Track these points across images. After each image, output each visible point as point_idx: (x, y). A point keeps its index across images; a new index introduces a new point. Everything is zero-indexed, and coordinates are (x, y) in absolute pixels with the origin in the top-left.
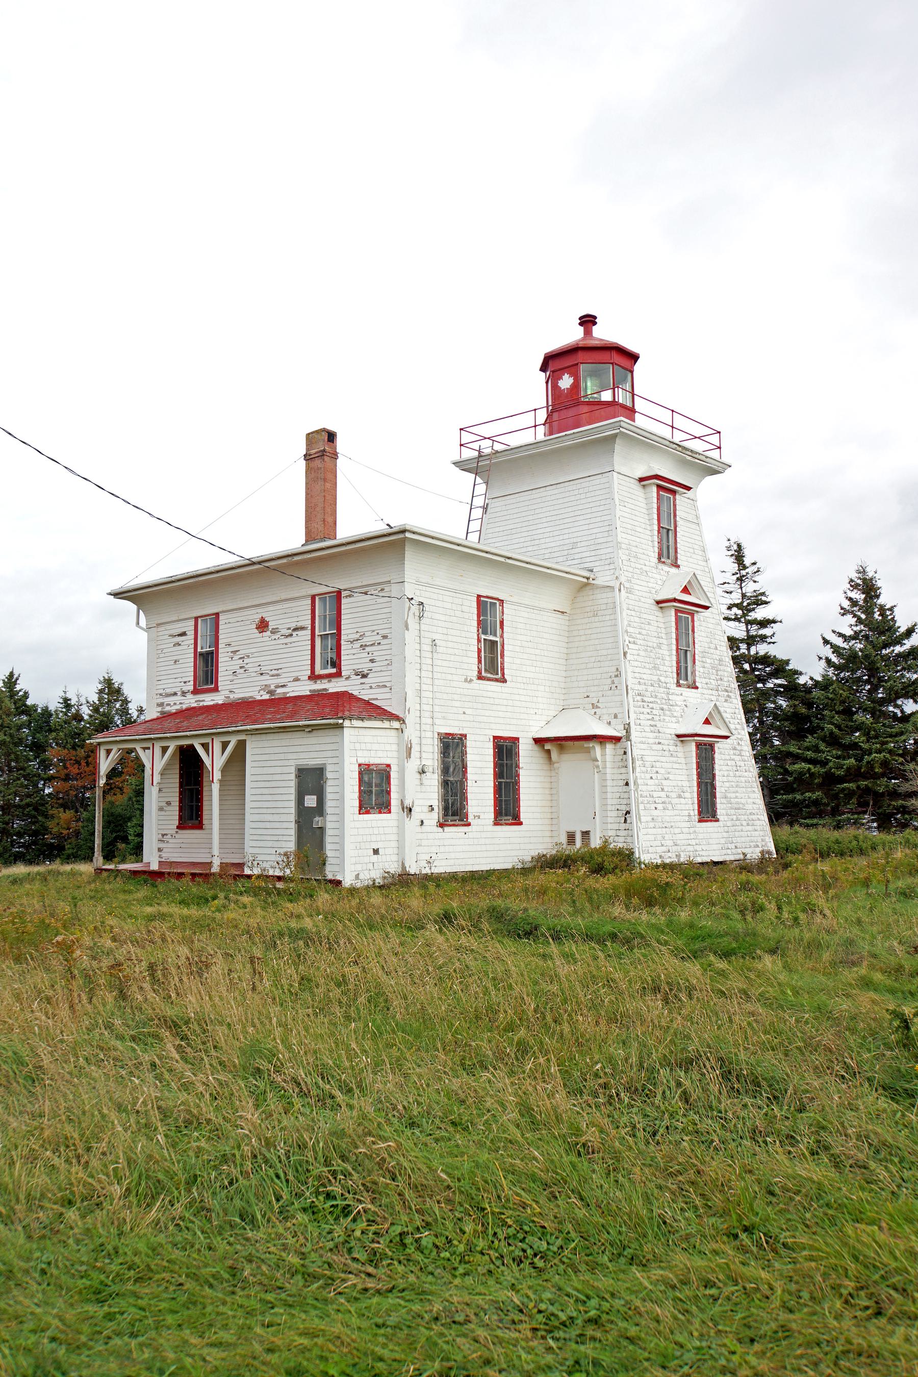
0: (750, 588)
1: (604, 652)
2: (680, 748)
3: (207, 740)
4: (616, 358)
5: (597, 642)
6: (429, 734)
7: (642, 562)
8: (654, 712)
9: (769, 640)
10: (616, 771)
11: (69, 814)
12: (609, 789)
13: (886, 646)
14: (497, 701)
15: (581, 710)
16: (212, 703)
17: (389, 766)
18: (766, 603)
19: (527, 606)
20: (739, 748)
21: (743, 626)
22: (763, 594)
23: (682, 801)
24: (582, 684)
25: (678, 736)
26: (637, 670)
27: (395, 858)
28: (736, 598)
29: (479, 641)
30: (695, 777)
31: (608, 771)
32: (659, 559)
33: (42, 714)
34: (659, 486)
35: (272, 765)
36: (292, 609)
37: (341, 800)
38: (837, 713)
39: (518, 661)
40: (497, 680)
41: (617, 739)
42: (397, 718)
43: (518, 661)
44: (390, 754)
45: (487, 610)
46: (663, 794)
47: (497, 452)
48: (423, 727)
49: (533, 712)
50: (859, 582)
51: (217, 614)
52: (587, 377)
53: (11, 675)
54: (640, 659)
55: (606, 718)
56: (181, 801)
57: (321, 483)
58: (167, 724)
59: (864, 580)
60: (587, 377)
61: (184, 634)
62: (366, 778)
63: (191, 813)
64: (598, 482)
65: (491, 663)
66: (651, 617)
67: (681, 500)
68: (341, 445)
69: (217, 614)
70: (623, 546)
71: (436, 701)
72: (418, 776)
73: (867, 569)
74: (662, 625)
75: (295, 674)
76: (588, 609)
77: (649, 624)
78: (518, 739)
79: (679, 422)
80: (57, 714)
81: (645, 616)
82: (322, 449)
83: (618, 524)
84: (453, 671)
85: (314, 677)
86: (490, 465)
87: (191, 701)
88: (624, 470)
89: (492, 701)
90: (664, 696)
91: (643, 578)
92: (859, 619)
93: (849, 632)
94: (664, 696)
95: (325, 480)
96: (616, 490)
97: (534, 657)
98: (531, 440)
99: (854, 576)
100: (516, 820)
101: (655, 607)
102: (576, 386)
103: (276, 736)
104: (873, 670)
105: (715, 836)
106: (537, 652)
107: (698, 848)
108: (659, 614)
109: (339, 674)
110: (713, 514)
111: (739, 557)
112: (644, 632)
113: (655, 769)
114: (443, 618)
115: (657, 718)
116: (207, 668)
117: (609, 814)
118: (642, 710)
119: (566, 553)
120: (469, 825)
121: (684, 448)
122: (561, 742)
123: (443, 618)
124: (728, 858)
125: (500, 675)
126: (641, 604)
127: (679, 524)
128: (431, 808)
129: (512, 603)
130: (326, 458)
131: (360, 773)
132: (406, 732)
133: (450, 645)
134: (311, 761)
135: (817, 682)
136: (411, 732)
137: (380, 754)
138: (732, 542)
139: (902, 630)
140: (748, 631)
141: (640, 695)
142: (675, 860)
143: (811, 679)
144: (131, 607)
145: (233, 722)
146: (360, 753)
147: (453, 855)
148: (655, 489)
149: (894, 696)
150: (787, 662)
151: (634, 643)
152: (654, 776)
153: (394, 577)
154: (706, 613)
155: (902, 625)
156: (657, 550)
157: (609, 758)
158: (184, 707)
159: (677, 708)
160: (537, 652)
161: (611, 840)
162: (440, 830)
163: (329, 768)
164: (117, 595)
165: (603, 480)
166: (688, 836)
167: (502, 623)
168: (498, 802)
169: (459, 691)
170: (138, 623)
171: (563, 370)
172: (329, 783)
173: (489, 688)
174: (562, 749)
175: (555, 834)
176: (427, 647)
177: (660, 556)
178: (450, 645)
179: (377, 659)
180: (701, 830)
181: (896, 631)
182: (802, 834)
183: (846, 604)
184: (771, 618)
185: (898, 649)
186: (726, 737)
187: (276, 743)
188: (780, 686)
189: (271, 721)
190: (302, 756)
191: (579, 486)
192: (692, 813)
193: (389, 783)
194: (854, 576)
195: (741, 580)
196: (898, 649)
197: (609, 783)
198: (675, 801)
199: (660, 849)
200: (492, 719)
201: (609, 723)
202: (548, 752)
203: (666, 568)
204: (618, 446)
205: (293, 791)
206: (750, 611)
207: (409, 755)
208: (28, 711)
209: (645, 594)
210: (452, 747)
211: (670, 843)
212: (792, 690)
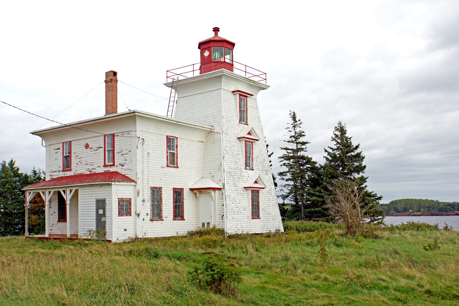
0: (298, 130)
1: (217, 157)
2: (245, 192)
3: (44, 191)
4: (225, 44)
5: (214, 153)
6: (147, 187)
7: (232, 123)
8: (235, 179)
9: (304, 150)
10: (219, 200)
11: (36, 216)
12: (217, 207)
13: (348, 153)
14: (175, 175)
15: (208, 178)
16: (69, 175)
17: (130, 199)
18: (304, 136)
19: (187, 140)
20: (270, 192)
21: (295, 145)
22: (303, 132)
23: (245, 211)
24: (209, 168)
25: (245, 188)
26: (228, 164)
27: (133, 232)
28: (293, 134)
29: (167, 152)
30: (251, 203)
31: (216, 200)
32: (240, 122)
33: (25, 177)
34: (240, 95)
35: (87, 198)
36: (97, 141)
37: (111, 211)
38: (328, 178)
39: (183, 160)
40: (175, 167)
41: (220, 189)
42: (134, 181)
43: (183, 160)
44: (131, 195)
45: (171, 142)
46: (237, 209)
47: (179, 80)
48: (144, 185)
49: (189, 179)
50: (339, 128)
51: (71, 142)
52: (215, 51)
53: (12, 161)
54: (230, 159)
55: (216, 181)
56: (59, 212)
57: (111, 92)
58: (52, 183)
59: (341, 127)
60: (215, 51)
61: (59, 149)
62: (121, 203)
63: (62, 217)
64: (216, 93)
65: (172, 161)
66: (235, 144)
67: (250, 100)
68: (119, 77)
69: (113, 135)
70: (225, 117)
71: (150, 175)
72: (142, 202)
73: (342, 123)
74: (240, 147)
75: (99, 165)
76: (211, 141)
78: (183, 189)
79: (248, 70)
80: (31, 177)
81: (232, 143)
82: (111, 78)
83: (223, 109)
84: (157, 164)
85: (105, 166)
86: (177, 86)
87: (62, 174)
88: (226, 88)
89: (172, 175)
90: (240, 173)
91: (233, 129)
92: (338, 142)
94: (240, 173)
95: (112, 90)
96: (222, 96)
97: (190, 159)
98: (192, 76)
99: (337, 125)
100: (258, 217)
101: (237, 140)
102: (210, 55)
103: (89, 188)
104: (343, 162)
105: (259, 224)
106: (192, 157)
107: (251, 228)
108: (239, 142)
109: (114, 165)
111: (294, 118)
112: (232, 149)
113: (234, 200)
114: (152, 144)
115: (236, 181)
117: (217, 216)
118: (230, 178)
119: (204, 119)
120: (163, 220)
121: (250, 80)
122: (200, 190)
123: (152, 144)
124: (263, 232)
125: (176, 165)
126: (231, 139)
127: (248, 109)
128: (148, 214)
129: (181, 139)
130: (113, 82)
131: (119, 201)
132: (137, 187)
133: (155, 154)
134: (101, 197)
135: (322, 166)
136: (139, 186)
137: (127, 194)
138: (292, 112)
139: (354, 146)
140: (297, 146)
141: (229, 173)
143: (320, 165)
144: (39, 139)
145: (74, 182)
146: (118, 194)
147: (156, 231)
148: (238, 95)
149: (350, 172)
150: (311, 158)
152: (234, 202)
153: (133, 129)
155: (354, 144)
156: (239, 119)
157: (216, 196)
158: (59, 176)
159: (245, 178)
160: (192, 157)
161: (217, 225)
162: (151, 222)
163: (107, 200)
164: (33, 133)
165: (218, 92)
166: (247, 224)
167: (177, 146)
168: (175, 212)
169: (159, 171)
170: (42, 144)
172: (107, 205)
173: (172, 170)
174: (200, 192)
175: (198, 223)
176: (146, 155)
177: (240, 120)
178: (155, 154)
179: (127, 159)
181: (351, 147)
182: (293, 223)
183: (334, 136)
184: (305, 141)
185: (353, 154)
186: (264, 188)
188: (309, 167)
189: (87, 182)
190: (98, 195)
191: (209, 94)
192: (249, 216)
193: (131, 205)
194: (337, 125)
195: (294, 127)
197: (217, 205)
198: (242, 212)
199: (235, 229)
200: (173, 182)
201: (218, 183)
202: (196, 193)
203: (242, 125)
204: (223, 79)
205: (95, 208)
206: (298, 139)
207: (138, 195)
208: (19, 175)
209: (233, 135)
210: (156, 193)
211: (240, 227)
212: (314, 169)
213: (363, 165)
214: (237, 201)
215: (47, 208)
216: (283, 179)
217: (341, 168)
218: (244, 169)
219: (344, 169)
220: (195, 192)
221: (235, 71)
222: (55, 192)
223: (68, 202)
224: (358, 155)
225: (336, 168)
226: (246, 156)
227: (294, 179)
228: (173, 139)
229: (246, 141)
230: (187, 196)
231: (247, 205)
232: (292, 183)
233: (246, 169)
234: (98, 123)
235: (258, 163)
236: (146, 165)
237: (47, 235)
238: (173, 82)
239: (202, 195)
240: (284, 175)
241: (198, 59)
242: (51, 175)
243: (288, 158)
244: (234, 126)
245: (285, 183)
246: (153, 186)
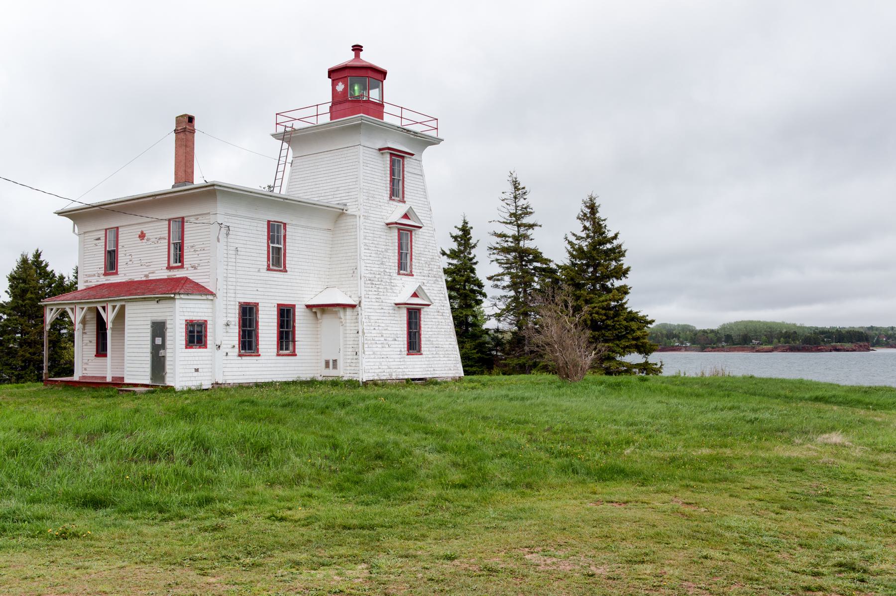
0: (521, 202)
4: (370, 73)
13: (600, 244)
19: (303, 226)
32: (391, 197)
35: (139, 318)
36: (158, 229)
37: (174, 340)
40: (280, 271)
41: (353, 306)
42: (212, 294)
45: (275, 232)
46: (382, 339)
51: (117, 228)
52: (356, 82)
60: (356, 82)
61: (99, 239)
63: (101, 350)
65: (277, 259)
67: (409, 163)
69: (117, 228)
79: (406, 114)
82: (186, 126)
85: (169, 268)
87: (104, 280)
101: (386, 227)
102: (345, 91)
103: (140, 303)
109: (182, 267)
110: (431, 168)
116: (111, 261)
121: (408, 131)
129: (292, 225)
134: (159, 318)
137: (200, 314)
142: (389, 377)
144: (69, 222)
148: (388, 156)
163: (168, 322)
171: (339, 79)
172: (168, 330)
187: (142, 307)
196: (609, 246)
202: (315, 313)
210: (248, 315)
213: (625, 267)
215: (77, 334)
216: (497, 286)
217: (591, 270)
219: (595, 271)
220: (314, 310)
221: (387, 119)
222: (89, 309)
223: (109, 325)
225: (582, 270)
226: (400, 254)
227: (513, 286)
229: (399, 229)
230: (302, 318)
231: (383, 334)
232: (512, 293)
233: (399, 274)
234: (159, 200)
236: (231, 267)
237: (76, 377)
238: (285, 131)
239: (325, 316)
240: (498, 280)
241: (327, 96)
242: (87, 282)
243: (506, 250)
245: (500, 292)
246: (243, 301)
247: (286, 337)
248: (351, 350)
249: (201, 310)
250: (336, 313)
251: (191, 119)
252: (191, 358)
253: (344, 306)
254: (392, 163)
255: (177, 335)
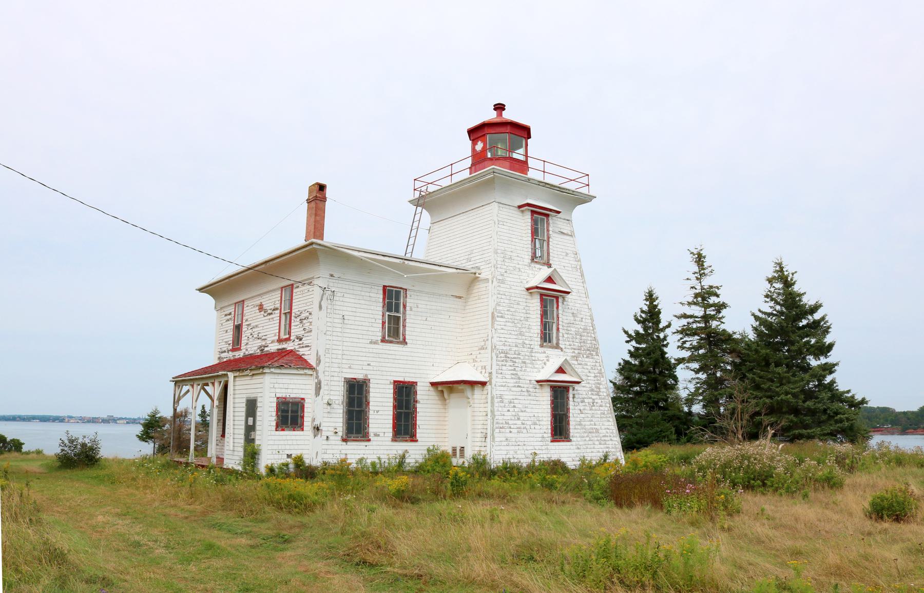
0: (707, 282)
19: (427, 293)
25: (538, 382)
32: (532, 260)
40: (398, 343)
41: (483, 384)
45: (393, 299)
46: (519, 422)
51: (243, 301)
52: (499, 138)
65: (394, 330)
67: (555, 224)
68: (329, 193)
77: (518, 304)
85: (280, 341)
87: (230, 356)
89: (393, 357)
93: (770, 310)
98: (450, 183)
101: (526, 293)
111: (699, 259)
112: (512, 310)
118: (504, 363)
120: (369, 440)
129: (414, 291)
133: (358, 319)
137: (295, 391)
148: (530, 213)
151: (502, 317)
152: (511, 409)
154: (569, 296)
159: (539, 362)
167: (405, 307)
172: (259, 409)
180: (553, 448)
192: (545, 435)
202: (442, 392)
210: (357, 392)
214: (520, 406)
218: (537, 348)
220: (440, 388)
221: (531, 174)
224: (816, 324)
228: (398, 293)
229: (541, 295)
235: (570, 336)
236: (340, 335)
239: (453, 395)
244: (520, 266)
247: (405, 425)
248: (479, 435)
249: (298, 386)
250: (462, 391)
251: (322, 188)
252: (282, 442)
253: (472, 384)
254: (535, 223)
255: (267, 415)
